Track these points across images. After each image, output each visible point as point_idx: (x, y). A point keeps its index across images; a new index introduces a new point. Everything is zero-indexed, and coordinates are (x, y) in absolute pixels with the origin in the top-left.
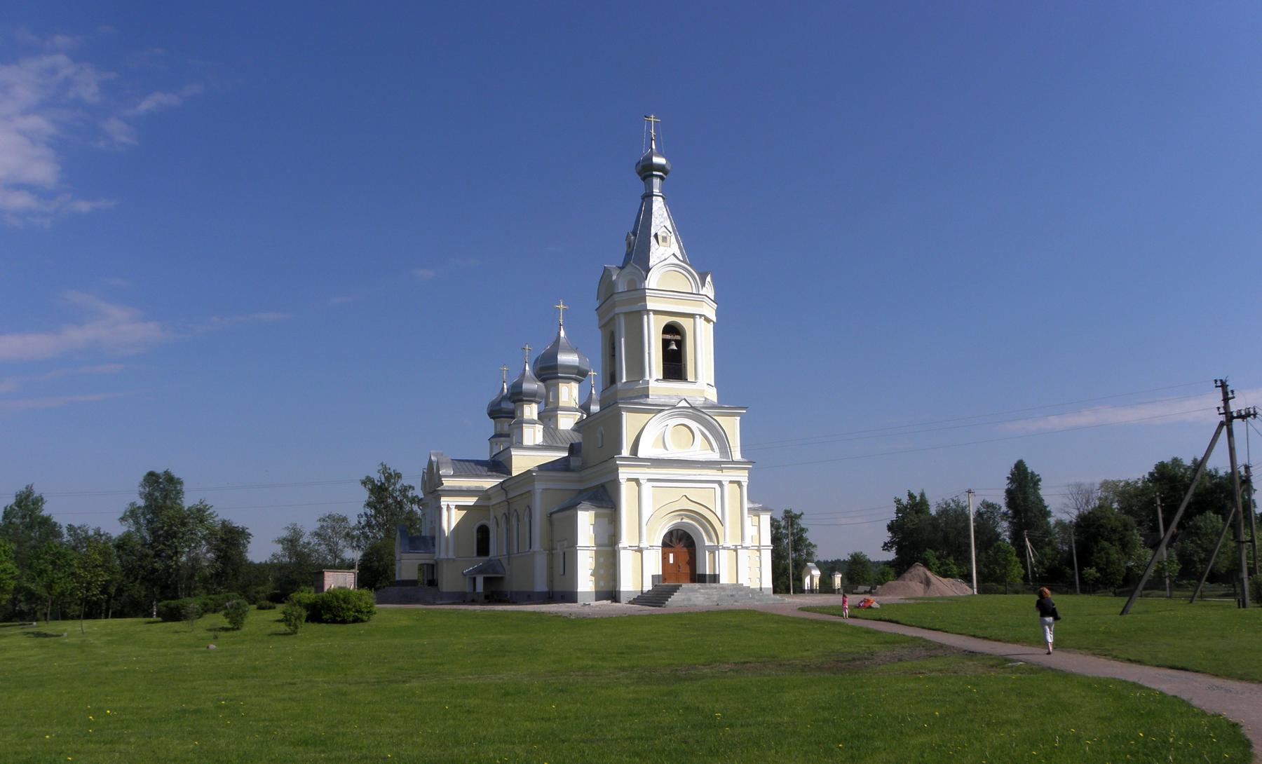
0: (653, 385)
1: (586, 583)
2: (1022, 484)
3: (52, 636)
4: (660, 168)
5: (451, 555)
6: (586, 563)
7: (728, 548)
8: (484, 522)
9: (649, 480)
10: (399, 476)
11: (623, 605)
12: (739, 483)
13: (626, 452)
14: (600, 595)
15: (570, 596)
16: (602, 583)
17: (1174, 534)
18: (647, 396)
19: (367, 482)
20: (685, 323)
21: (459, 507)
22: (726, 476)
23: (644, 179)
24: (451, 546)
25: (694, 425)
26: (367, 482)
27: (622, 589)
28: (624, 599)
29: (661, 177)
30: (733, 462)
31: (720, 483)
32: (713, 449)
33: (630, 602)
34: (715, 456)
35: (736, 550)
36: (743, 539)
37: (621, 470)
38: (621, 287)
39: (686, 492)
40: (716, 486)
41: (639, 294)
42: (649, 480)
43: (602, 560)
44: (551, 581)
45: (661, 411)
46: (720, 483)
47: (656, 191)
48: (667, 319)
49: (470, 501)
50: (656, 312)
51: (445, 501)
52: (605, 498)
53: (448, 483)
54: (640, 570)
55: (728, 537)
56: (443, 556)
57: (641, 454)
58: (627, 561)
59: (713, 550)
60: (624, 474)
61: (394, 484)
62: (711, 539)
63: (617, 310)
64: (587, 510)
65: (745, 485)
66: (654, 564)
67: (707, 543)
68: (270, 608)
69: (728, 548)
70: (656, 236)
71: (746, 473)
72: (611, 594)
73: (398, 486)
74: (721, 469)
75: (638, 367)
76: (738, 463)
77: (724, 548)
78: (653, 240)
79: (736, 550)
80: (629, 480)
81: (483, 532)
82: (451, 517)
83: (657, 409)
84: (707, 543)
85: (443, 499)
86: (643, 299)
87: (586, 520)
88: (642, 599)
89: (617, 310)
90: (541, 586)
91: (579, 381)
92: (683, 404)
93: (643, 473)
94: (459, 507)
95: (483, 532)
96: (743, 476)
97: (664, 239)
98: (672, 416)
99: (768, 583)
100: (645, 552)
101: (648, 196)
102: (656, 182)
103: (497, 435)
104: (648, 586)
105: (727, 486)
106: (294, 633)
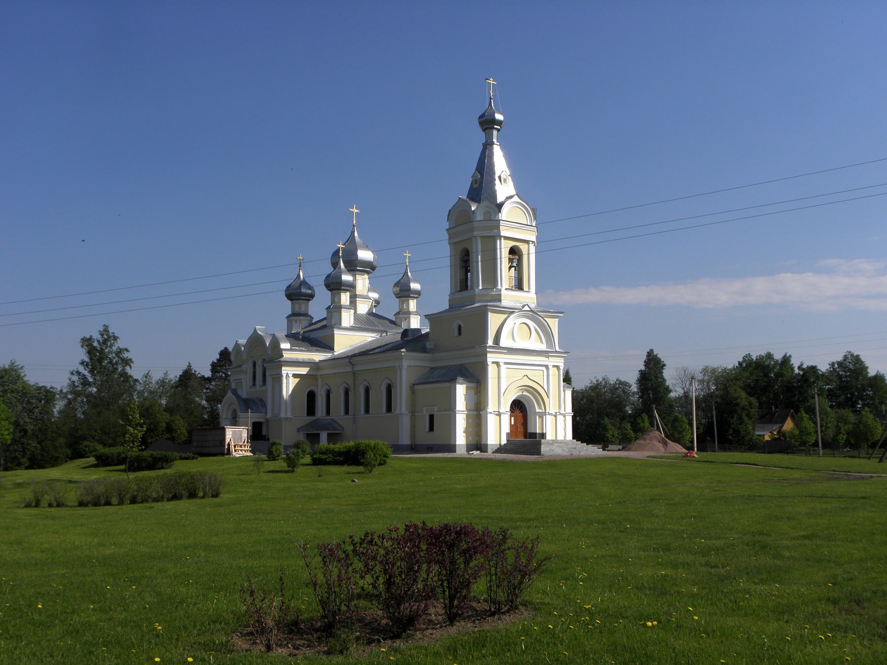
0: (504, 293)
1: (461, 439)
2: (653, 365)
3: (269, 472)
4: (500, 123)
5: (289, 415)
6: (461, 422)
7: (551, 414)
8: (313, 388)
9: (506, 363)
10: (115, 338)
11: (489, 454)
12: (558, 367)
13: (490, 342)
14: (470, 447)
15: (452, 448)
16: (470, 438)
17: (763, 404)
18: (500, 301)
19: (87, 342)
20: (523, 247)
21: (295, 376)
22: (551, 361)
23: (484, 130)
24: (289, 409)
25: (531, 324)
26: (87, 342)
27: (489, 443)
28: (490, 450)
29: (498, 130)
30: (556, 352)
31: (547, 367)
32: (542, 342)
33: (493, 452)
34: (543, 347)
35: (555, 416)
36: (560, 408)
37: (489, 355)
38: (479, 217)
39: (526, 372)
40: (544, 368)
41: (496, 225)
42: (506, 363)
43: (470, 421)
44: (413, 436)
45: (512, 313)
46: (547, 367)
47: (495, 140)
48: (512, 244)
49: (304, 371)
50: (506, 238)
51: (285, 370)
52: (477, 379)
53: (287, 355)
54: (498, 430)
55: (552, 408)
56: (283, 415)
57: (503, 343)
58: (492, 422)
59: (542, 415)
60: (491, 358)
61: (111, 345)
62: (540, 408)
63: (476, 233)
64: (462, 384)
65: (562, 368)
66: (506, 422)
67: (538, 410)
68: (193, 458)
69: (551, 414)
70: (500, 178)
71: (562, 360)
72: (477, 443)
73: (114, 348)
74: (548, 357)
75: (492, 278)
76: (559, 352)
77: (549, 414)
78: (497, 182)
79: (555, 416)
80: (554, 366)
81: (311, 397)
82: (289, 385)
83: (510, 311)
84: (538, 410)
85: (283, 368)
86: (498, 227)
87: (461, 390)
88: (500, 449)
89: (476, 233)
90: (406, 440)
91: (368, 273)
92: (526, 308)
93: (502, 358)
94: (295, 376)
95: (311, 397)
96: (560, 362)
97: (505, 180)
98: (519, 316)
99: (570, 436)
100: (502, 416)
101: (487, 146)
102: (495, 132)
103: (294, 314)
104: (504, 441)
105: (551, 370)
106: (293, 471)
